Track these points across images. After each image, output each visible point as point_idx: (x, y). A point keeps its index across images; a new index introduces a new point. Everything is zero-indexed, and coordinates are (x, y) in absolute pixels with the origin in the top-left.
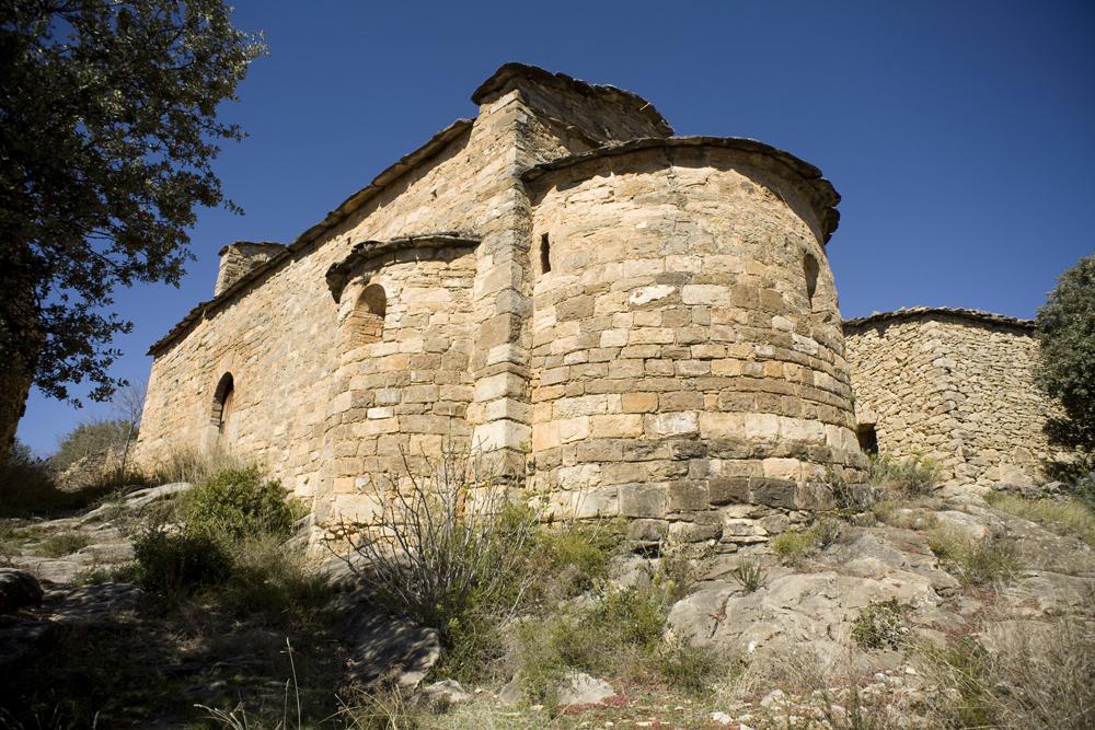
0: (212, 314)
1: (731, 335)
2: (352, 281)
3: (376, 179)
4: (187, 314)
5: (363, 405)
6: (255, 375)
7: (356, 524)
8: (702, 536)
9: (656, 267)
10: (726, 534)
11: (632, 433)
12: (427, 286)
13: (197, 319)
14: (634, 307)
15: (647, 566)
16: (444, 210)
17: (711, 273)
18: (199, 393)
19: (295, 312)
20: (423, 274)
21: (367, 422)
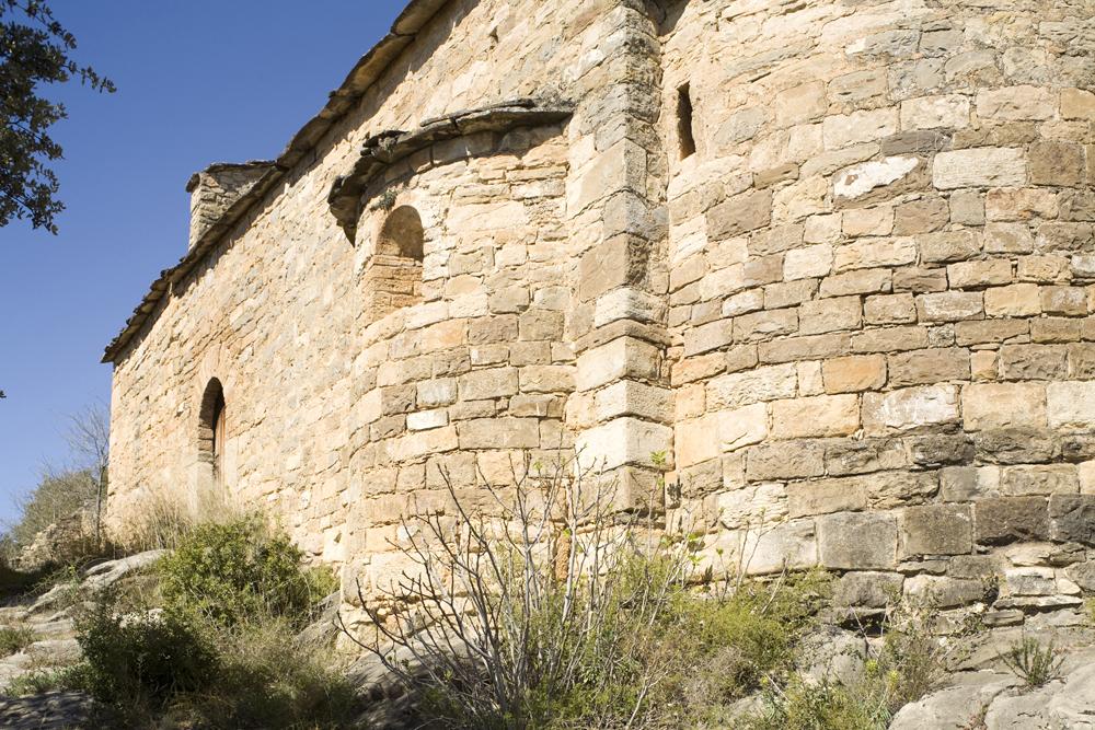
0: (181, 288)
1: (1024, 239)
2: (369, 206)
3: (398, 20)
4: (147, 292)
5: (402, 409)
6: (251, 376)
7: (404, 598)
8: (960, 597)
9: (883, 124)
10: (1003, 593)
11: (840, 427)
12: (487, 200)
13: (162, 297)
14: (842, 203)
15: (862, 650)
16: (512, 62)
17: (987, 124)
18: (179, 414)
19: (298, 270)
20: (480, 181)
21: (408, 436)
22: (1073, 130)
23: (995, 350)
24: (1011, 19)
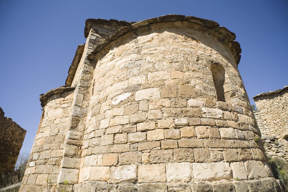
3: (69, 72)
14: (113, 107)
22: (175, 81)
23: (149, 152)
24: (157, 56)
